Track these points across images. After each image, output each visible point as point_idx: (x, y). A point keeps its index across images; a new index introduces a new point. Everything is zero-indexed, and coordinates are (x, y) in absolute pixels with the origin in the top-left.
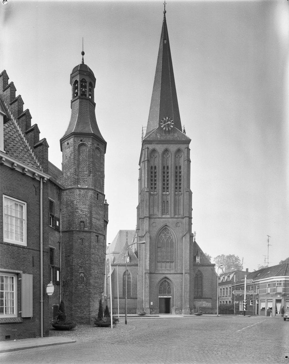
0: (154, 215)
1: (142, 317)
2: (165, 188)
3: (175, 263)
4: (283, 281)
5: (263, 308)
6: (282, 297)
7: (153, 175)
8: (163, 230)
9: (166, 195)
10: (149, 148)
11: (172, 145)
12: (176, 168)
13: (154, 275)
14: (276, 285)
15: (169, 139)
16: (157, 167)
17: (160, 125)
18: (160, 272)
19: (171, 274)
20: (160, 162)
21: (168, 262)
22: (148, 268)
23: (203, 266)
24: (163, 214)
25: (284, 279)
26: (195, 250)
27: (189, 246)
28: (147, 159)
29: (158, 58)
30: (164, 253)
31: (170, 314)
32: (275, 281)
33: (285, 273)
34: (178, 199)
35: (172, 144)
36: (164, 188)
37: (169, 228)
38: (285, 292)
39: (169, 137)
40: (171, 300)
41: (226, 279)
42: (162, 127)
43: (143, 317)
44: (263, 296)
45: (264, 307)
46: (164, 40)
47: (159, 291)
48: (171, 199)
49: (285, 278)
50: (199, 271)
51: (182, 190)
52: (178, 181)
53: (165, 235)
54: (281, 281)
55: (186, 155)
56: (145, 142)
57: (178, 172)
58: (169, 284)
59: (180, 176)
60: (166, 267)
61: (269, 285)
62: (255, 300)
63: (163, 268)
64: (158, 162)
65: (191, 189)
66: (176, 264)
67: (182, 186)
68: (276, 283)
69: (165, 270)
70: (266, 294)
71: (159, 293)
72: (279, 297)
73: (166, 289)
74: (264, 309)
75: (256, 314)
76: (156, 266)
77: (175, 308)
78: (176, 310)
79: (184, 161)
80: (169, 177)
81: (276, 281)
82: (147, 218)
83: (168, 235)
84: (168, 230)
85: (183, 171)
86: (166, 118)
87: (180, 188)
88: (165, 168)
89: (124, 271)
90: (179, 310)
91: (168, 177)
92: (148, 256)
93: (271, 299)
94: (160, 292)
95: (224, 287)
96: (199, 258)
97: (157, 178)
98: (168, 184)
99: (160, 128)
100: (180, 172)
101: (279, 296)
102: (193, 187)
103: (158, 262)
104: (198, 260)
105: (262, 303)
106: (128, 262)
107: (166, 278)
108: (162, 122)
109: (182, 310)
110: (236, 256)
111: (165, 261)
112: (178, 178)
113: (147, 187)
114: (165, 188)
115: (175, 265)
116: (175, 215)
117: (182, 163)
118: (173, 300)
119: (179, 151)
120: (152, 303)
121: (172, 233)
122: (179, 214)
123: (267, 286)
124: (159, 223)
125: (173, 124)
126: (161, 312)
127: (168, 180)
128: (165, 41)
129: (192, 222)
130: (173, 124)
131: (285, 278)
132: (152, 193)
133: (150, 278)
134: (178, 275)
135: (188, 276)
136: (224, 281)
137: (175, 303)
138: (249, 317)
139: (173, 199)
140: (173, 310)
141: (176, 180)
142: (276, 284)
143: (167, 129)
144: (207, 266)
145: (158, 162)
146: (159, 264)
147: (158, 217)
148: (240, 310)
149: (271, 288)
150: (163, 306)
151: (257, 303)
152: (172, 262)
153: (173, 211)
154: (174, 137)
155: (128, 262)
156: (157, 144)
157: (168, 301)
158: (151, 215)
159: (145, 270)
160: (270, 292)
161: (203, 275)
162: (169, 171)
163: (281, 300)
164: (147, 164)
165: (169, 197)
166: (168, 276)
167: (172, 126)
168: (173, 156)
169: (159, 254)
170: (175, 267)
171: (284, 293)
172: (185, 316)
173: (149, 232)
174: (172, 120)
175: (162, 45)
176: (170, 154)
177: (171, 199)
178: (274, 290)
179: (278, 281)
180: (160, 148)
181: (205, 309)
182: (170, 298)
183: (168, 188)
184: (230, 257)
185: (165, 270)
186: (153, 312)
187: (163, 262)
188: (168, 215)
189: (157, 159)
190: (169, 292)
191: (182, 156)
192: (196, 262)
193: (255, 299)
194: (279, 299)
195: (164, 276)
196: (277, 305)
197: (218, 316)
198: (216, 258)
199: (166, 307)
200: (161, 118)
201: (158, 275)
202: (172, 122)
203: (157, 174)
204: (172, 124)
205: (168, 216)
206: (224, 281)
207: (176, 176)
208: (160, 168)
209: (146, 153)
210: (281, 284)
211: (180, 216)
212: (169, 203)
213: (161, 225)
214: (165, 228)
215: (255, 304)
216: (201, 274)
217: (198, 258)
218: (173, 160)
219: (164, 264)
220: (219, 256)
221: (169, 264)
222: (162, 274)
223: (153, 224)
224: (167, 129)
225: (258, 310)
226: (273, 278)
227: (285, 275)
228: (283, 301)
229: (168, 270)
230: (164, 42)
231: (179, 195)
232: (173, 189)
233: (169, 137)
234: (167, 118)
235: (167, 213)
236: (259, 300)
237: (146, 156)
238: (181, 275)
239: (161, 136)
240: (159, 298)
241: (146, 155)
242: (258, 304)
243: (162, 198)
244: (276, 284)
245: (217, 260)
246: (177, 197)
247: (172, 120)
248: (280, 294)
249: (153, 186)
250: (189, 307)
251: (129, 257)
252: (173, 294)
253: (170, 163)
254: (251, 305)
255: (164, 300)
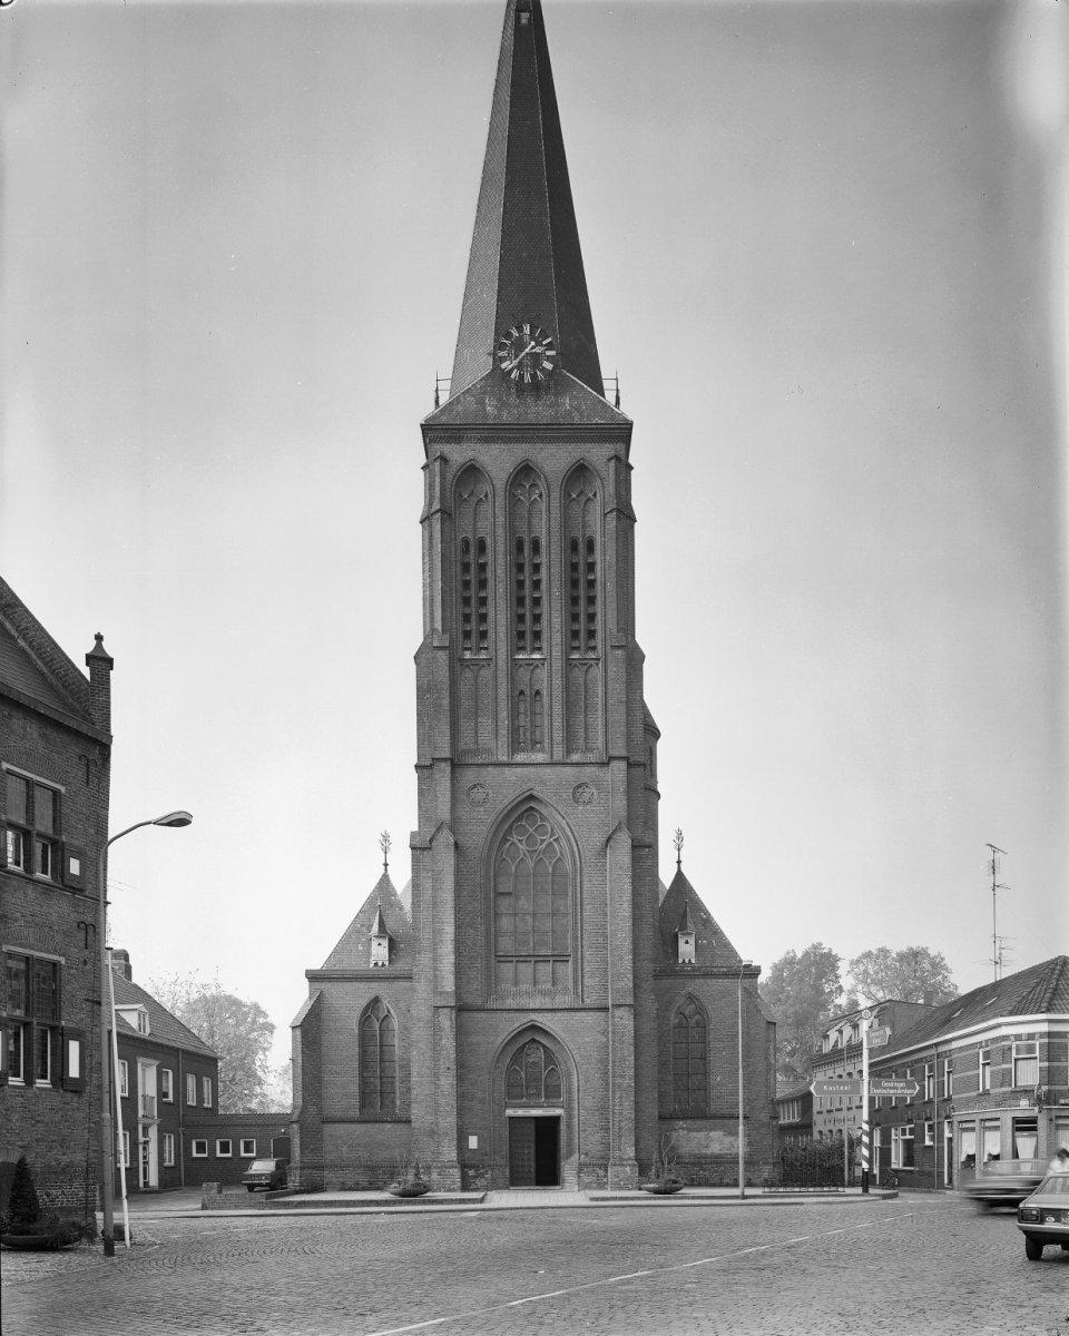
0: (476, 752)
1: (408, 1203)
2: (525, 633)
3: (575, 962)
4: (1042, 1035)
5: (968, 1156)
6: (1036, 1109)
7: (472, 576)
8: (519, 819)
9: (530, 663)
10: (449, 457)
11: (551, 448)
12: (574, 546)
13: (483, 1015)
14: (1014, 1055)
15: (534, 421)
16: (489, 541)
17: (498, 361)
18: (510, 1003)
19: (559, 1010)
20: (501, 520)
21: (545, 959)
22: (449, 984)
23: (707, 975)
24: (515, 746)
25: (1044, 1028)
26: (675, 913)
27: (628, 887)
28: (438, 507)
29: (496, 86)
30: (528, 917)
31: (557, 1187)
32: (1005, 1038)
33: (1051, 999)
34: (581, 681)
35: (551, 440)
36: (521, 635)
37: (544, 811)
38: (1049, 1083)
39: (538, 411)
40: (563, 1127)
41: (846, 1038)
42: (503, 366)
43: (414, 1203)
44: (967, 1103)
45: (971, 1153)
46: (519, 11)
47: (509, 1086)
48: (549, 680)
49: (1050, 1021)
50: (691, 998)
51: (599, 641)
52: (582, 602)
53: (530, 840)
54: (1031, 1036)
55: (611, 489)
56: (433, 431)
57: (582, 567)
58: (550, 1058)
59: (591, 584)
60: (535, 983)
61: (987, 1055)
62: (940, 1124)
63: (524, 987)
64: (491, 522)
65: (639, 638)
66: (580, 965)
67: (598, 625)
68: (1014, 1046)
69: (530, 996)
70: (975, 1094)
71: (510, 1095)
72: (1024, 1107)
73: (538, 1079)
74: (971, 1158)
75: (946, 1181)
76: (491, 981)
77: (576, 1164)
78: (581, 1168)
79: (606, 514)
80: (544, 586)
81: (1012, 1038)
82: (443, 764)
83: (543, 841)
84: (543, 818)
85: (604, 558)
86: (520, 329)
87: (591, 634)
88: (523, 549)
89: (364, 1003)
90: (597, 1169)
91: (537, 585)
92: (449, 930)
93: (994, 1116)
94: (514, 1093)
95: (839, 1071)
96: (692, 941)
97: (489, 593)
98: (537, 618)
99: (498, 376)
100: (591, 567)
101: (1024, 1103)
102: (646, 634)
103: (502, 959)
104: (687, 949)
105: (965, 1135)
106: (383, 965)
107: (534, 1028)
108: (501, 346)
109: (606, 1171)
110: (932, 952)
111: (531, 952)
112: (582, 593)
113: (440, 628)
114: (525, 633)
115: (575, 970)
116: (569, 752)
117: (598, 521)
118: (569, 1127)
119: (580, 471)
120: (473, 1142)
121: (558, 833)
122: (588, 749)
123: (981, 1061)
124: (503, 786)
125: (553, 353)
126: (516, 1181)
127: (537, 602)
128: (525, 17)
129: (660, 789)
130: (553, 353)
131: (1050, 1021)
132: (468, 655)
133: (460, 1031)
134: (590, 1017)
135: (625, 1020)
136: (840, 1047)
137: (581, 1138)
138: (885, 1197)
139: (558, 682)
140: (568, 1170)
141: (575, 600)
142: (1010, 1049)
143: (527, 379)
144: (726, 975)
145: (491, 522)
146: (507, 970)
147: (494, 760)
148: (893, 1166)
149: (994, 1068)
150: (529, 1152)
151: (947, 1134)
152: (560, 958)
153: (558, 736)
154: (557, 412)
155: (383, 965)
156: (487, 440)
157: (547, 1131)
158: (466, 752)
159: (437, 992)
160: (992, 1087)
161: (711, 1014)
162: (543, 559)
163: (1034, 1120)
164: (439, 526)
165: (543, 673)
166: (543, 1020)
167: (548, 366)
168: (556, 494)
169: (506, 923)
170: (575, 982)
171: (1045, 1088)
172: (597, 1199)
173: (454, 825)
174: (550, 339)
175: (511, 31)
176: (542, 484)
177: (549, 680)
178: (1005, 1078)
179: (1018, 1037)
180: (498, 461)
181: (719, 1164)
182: (557, 1119)
183: (537, 635)
184: (915, 956)
185: (530, 996)
186: (481, 1182)
187: (525, 959)
188: (542, 750)
189: (486, 508)
190: (553, 1093)
191: (595, 495)
192: (680, 961)
193: (940, 1120)
194: (1027, 1114)
195: (522, 1020)
196: (1020, 1141)
197: (745, 1197)
198: (858, 961)
199: (541, 1155)
200: (501, 332)
201: (499, 1014)
202: (550, 346)
203: (489, 574)
204: (548, 353)
205: (540, 757)
206: (840, 1047)
207: (575, 583)
208: (501, 548)
209: (438, 480)
210: (1031, 1049)
211: (591, 757)
212: (546, 699)
213: (512, 797)
214: (526, 808)
215: (940, 1140)
216: (700, 1010)
217: (687, 942)
218: (556, 513)
219: (526, 969)
220: (868, 955)
221: (549, 967)
222: (537, 1010)
223: (475, 790)
224: (527, 379)
225: (950, 1165)
226: (999, 1026)
227: (1048, 1010)
228: (1042, 1123)
229: (543, 993)
230: (518, 19)
231: (586, 665)
232: (557, 638)
233: (538, 411)
234: (527, 329)
235: (534, 744)
236: (956, 1123)
237: (438, 494)
238: (598, 1014)
239: (502, 405)
240: (511, 1118)
241: (438, 488)
242: (950, 1140)
243: (512, 680)
244: (1014, 1051)
245: (862, 968)
246: (578, 674)
247: (550, 339)
248: (1027, 1092)
249: (473, 626)
250: (632, 1154)
251: (385, 943)
252: (570, 1100)
253: (545, 525)
254: (928, 1142)
255: (531, 1129)
